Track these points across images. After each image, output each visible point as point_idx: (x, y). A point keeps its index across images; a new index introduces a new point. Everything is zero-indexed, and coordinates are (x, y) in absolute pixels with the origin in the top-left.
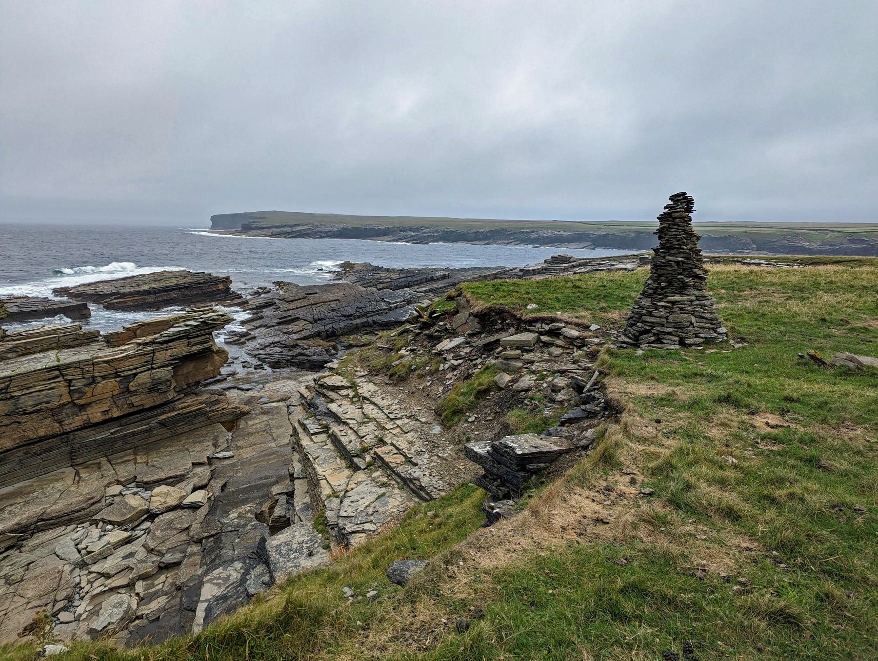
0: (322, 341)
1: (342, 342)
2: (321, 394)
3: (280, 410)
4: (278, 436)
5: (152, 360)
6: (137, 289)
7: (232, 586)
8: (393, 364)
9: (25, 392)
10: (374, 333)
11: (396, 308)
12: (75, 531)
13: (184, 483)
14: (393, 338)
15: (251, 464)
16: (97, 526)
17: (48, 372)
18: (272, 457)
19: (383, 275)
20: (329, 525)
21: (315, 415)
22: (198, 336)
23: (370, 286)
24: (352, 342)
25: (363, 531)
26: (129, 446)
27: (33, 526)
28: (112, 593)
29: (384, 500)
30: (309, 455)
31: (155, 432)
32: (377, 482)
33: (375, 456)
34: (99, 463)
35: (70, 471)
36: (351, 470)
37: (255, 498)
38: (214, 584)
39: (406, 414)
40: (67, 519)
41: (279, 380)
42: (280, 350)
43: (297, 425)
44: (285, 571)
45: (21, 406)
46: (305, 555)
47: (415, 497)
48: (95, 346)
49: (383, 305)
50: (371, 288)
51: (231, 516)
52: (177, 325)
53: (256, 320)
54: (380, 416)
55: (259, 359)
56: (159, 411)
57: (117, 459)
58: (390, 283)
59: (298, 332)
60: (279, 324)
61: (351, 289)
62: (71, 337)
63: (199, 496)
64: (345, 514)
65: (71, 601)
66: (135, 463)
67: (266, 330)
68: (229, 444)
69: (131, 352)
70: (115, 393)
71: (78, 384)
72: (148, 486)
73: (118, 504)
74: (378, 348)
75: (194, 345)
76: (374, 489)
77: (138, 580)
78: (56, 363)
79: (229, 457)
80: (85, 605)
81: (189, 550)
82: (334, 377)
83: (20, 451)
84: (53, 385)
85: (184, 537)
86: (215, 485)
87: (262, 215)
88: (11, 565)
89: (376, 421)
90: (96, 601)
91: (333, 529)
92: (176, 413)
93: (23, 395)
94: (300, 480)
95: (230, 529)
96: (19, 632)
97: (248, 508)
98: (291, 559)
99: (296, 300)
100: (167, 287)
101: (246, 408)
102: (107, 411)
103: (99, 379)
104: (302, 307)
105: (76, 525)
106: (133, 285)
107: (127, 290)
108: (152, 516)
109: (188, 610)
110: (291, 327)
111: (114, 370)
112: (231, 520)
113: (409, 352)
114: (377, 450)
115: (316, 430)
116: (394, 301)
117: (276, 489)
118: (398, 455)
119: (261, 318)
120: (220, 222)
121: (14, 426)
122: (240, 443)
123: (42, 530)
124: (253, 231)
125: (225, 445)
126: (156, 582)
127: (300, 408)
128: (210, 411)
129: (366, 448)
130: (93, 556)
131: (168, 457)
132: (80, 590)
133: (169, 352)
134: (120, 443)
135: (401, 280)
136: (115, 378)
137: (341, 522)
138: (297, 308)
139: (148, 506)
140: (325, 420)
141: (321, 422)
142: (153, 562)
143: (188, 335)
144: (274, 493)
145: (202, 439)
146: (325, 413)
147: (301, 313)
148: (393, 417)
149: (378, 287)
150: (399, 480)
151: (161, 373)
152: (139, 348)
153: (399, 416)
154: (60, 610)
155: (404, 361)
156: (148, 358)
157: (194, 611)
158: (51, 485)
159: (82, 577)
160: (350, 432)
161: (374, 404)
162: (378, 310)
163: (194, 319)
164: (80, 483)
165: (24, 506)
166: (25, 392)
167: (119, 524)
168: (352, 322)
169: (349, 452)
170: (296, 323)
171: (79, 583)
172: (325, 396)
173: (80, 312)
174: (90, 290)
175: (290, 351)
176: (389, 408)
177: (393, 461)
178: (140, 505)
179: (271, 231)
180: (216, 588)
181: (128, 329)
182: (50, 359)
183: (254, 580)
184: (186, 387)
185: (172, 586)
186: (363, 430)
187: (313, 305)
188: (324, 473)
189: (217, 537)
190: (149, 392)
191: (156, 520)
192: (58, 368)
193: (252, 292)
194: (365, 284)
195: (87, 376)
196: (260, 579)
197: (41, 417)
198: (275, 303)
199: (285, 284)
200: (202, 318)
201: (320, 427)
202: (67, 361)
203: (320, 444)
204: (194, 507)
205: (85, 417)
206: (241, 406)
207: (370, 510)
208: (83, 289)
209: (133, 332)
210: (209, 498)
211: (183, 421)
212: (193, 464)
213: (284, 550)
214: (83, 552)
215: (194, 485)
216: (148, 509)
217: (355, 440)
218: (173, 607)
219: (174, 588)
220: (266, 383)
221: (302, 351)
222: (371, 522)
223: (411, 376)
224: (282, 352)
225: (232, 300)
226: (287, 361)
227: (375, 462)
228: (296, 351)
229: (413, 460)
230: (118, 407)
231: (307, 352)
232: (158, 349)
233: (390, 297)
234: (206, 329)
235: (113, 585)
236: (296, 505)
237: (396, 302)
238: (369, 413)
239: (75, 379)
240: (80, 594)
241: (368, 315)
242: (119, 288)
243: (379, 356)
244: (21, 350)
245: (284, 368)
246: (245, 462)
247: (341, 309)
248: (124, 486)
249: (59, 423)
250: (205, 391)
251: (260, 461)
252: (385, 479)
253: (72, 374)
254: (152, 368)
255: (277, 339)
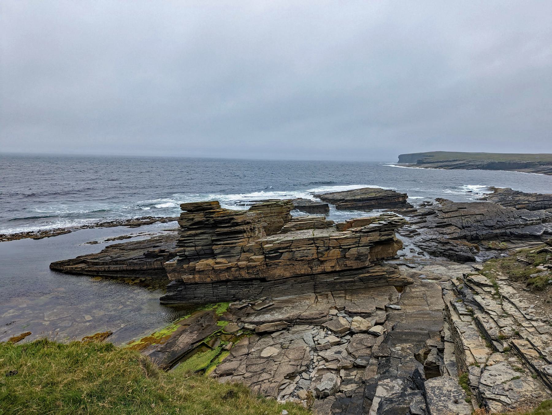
0: (467, 242)
1: (483, 245)
2: (469, 287)
3: (434, 286)
4: (432, 303)
5: (359, 242)
6: (353, 198)
7: (396, 395)
8: (531, 276)
9: (298, 249)
10: (510, 241)
11: (532, 224)
12: (313, 329)
13: (371, 318)
14: (532, 255)
15: (412, 317)
16: (324, 330)
17: (309, 240)
18: (426, 316)
19: (522, 198)
20: (471, 386)
21: (463, 301)
22: (385, 231)
23: (510, 206)
24: (491, 246)
25: (499, 401)
26: (342, 288)
27: (295, 321)
28: (328, 371)
29: (519, 383)
30: (457, 329)
31: (357, 283)
32: (512, 366)
33: (512, 345)
34: (327, 295)
35: (313, 295)
36: (490, 349)
37: (414, 341)
38: (384, 388)
39: (541, 318)
40: (310, 321)
41: (434, 265)
42: (436, 244)
43: (449, 304)
44: (437, 407)
45: (296, 256)
46: (452, 401)
47: (547, 389)
48: (331, 229)
49: (520, 222)
50: (510, 207)
51: (397, 348)
52: (374, 223)
53: (421, 223)
54: (517, 314)
55: (421, 248)
56: (360, 271)
57: (336, 294)
58: (527, 205)
59: (450, 234)
60: (437, 227)
61: (494, 207)
62: (320, 223)
63: (378, 329)
64: (484, 383)
65: (308, 368)
66: (345, 299)
67: (427, 230)
68: (399, 301)
69: (349, 235)
70: (339, 257)
71: (321, 249)
72: (351, 314)
73: (335, 320)
74: (518, 260)
75: (383, 236)
76: (510, 371)
77: (342, 369)
78: (312, 237)
79: (398, 309)
80: (315, 373)
81: (371, 361)
82: (479, 276)
83: (293, 279)
84: (310, 248)
85: (368, 351)
86: (388, 324)
87: (431, 154)
88: (284, 338)
89: (514, 317)
90: (320, 373)
91: (474, 389)
92: (369, 275)
93: (296, 251)
94: (448, 343)
95: (396, 356)
96: (285, 375)
97: (408, 346)
98: (442, 400)
99: (450, 212)
100: (370, 198)
101: (411, 280)
102: (334, 266)
103: (331, 248)
104: (454, 217)
105: (313, 326)
106: (352, 195)
107: (348, 198)
108: (352, 333)
109: (368, 398)
110: (445, 230)
111: (339, 244)
112: (397, 351)
113: (546, 269)
114: (514, 341)
115: (463, 312)
116: (531, 219)
117: (429, 342)
118: (532, 350)
119: (425, 221)
120: (403, 159)
121: (291, 266)
122: (406, 302)
123: (298, 324)
124: (424, 165)
125: (396, 301)
126: (351, 374)
127: (451, 293)
128: (388, 277)
129: (504, 336)
130: (320, 346)
131: (363, 300)
132: (313, 364)
133: (369, 238)
134: (338, 286)
135: (538, 202)
136: (339, 249)
137: (482, 388)
138: (450, 217)
139: (350, 327)
140: (471, 306)
141: (468, 307)
142: (350, 361)
143: (380, 229)
144: (428, 345)
145: (383, 293)
146: (471, 301)
147: (453, 221)
148: (529, 318)
149: (517, 207)
150: (533, 371)
151: (364, 250)
152: (353, 234)
153: (534, 318)
154: (303, 371)
155: (542, 275)
156: (357, 240)
157: (372, 400)
158: (304, 301)
159: (313, 356)
160: (491, 320)
161: (512, 303)
162: (516, 225)
163: (384, 220)
164: (318, 304)
165: (292, 308)
166: (298, 249)
167: (335, 333)
168: (493, 231)
169: (489, 336)
170: (449, 227)
171: (313, 359)
172: (471, 288)
173: (324, 209)
174: (330, 197)
175: (443, 246)
176: (526, 310)
177: (528, 353)
178: (346, 325)
179: (436, 165)
180: (385, 391)
181: (348, 222)
182: (309, 234)
183: (415, 404)
184: (376, 260)
185: (360, 380)
186: (502, 322)
187: (463, 216)
188: (469, 346)
189: (388, 358)
190: (356, 260)
191: (354, 336)
192: (313, 239)
193: (420, 204)
194: (506, 204)
195: (326, 245)
196: (419, 405)
197: (303, 264)
198: (435, 213)
199: (443, 200)
200: (389, 220)
201: (467, 310)
202: (318, 236)
203: (467, 323)
204: (375, 335)
205: (323, 268)
206: (408, 278)
207: (506, 387)
208: (327, 196)
209: (350, 224)
210: (384, 332)
211: (373, 280)
212: (376, 308)
213: (437, 392)
214: (316, 342)
215: (376, 321)
216: (350, 328)
217: (495, 328)
218: (360, 393)
219: (361, 381)
220: (425, 265)
221: (452, 247)
222: (507, 396)
223: (547, 288)
224: (437, 246)
225: (407, 208)
226: (441, 252)
227: (511, 349)
228: (448, 247)
229: (547, 358)
230: (339, 265)
231: (455, 249)
232: (363, 236)
233: (527, 216)
234: (391, 227)
235: (329, 367)
236: (445, 360)
237: (532, 220)
238: (508, 310)
239: (320, 246)
240: (313, 366)
241: (507, 228)
242: (344, 197)
243: (518, 267)
244: (298, 227)
245: (438, 257)
246: (408, 315)
247: (484, 221)
248: (338, 311)
249: (311, 268)
250: (386, 264)
251: (418, 317)
252: (520, 366)
253: (320, 243)
254: (359, 246)
255: (434, 237)
